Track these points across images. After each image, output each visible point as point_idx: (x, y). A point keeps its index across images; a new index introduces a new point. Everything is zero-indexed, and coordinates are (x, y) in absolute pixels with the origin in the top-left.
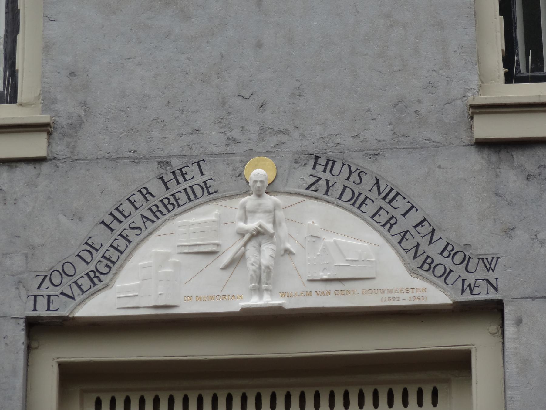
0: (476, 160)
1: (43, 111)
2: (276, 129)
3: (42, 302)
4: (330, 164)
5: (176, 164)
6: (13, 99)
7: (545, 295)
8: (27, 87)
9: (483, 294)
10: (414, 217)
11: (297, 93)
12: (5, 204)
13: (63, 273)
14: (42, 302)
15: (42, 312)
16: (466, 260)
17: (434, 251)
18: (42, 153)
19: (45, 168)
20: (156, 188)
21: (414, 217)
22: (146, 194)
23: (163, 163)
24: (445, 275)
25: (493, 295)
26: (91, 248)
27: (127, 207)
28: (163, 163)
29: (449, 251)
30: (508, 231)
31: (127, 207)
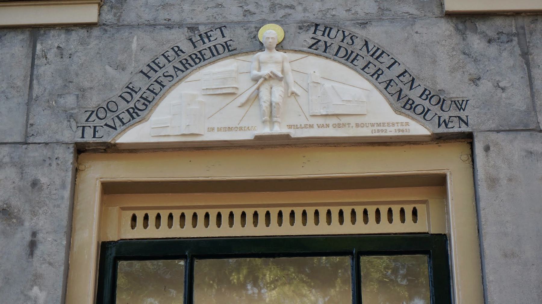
0: (446, 27)
2: (284, 4)
3: (89, 132)
4: (327, 29)
5: (202, 29)
9: (456, 128)
10: (397, 70)
14: (89, 132)
15: (89, 138)
19: (96, 32)
20: (187, 47)
21: (397, 70)
22: (178, 51)
25: (464, 129)
26: (131, 90)
27: (162, 61)
28: (192, 28)
29: (426, 94)
31: (162, 61)
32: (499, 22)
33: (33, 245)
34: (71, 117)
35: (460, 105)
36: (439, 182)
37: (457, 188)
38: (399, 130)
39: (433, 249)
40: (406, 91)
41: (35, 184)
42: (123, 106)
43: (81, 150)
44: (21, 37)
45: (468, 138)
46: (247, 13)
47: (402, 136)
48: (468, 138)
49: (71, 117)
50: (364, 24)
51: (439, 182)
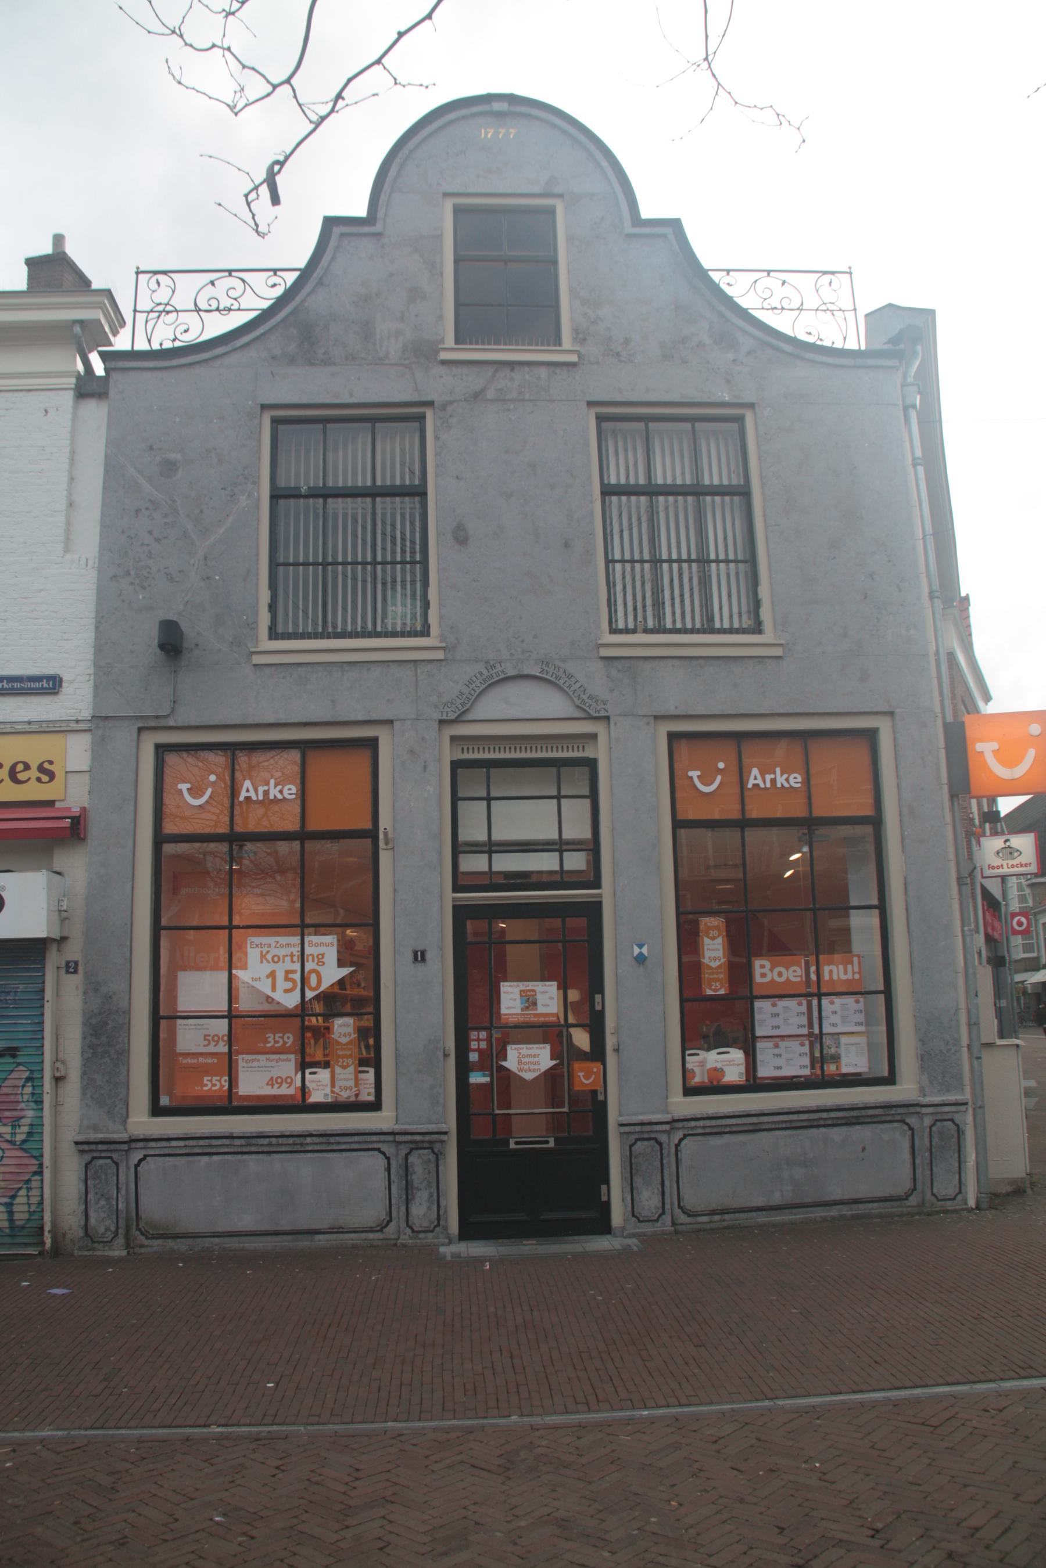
0: (600, 664)
1: (441, 641)
2: (304, 490)
3: (445, 714)
4: (548, 664)
5: (492, 663)
6: (428, 635)
7: (3, 394)
8: (434, 630)
9: (603, 714)
10: (578, 685)
11: (535, 637)
12: (172, 644)
13: (452, 703)
14: (445, 714)
15: (444, 717)
16: (597, 701)
17: (585, 697)
18: (442, 658)
19: (444, 663)
20: (485, 672)
21: (578, 685)
22: (481, 674)
23: (487, 662)
24: (775, 342)
25: (606, 714)
26: (462, 694)
27: (474, 679)
28: (487, 662)
29: (591, 697)
30: (612, 690)
31: (474, 679)
32: (623, 661)
33: (425, 767)
34: (436, 706)
35: (605, 703)
36: (594, 737)
37: (602, 739)
38: (253, 1061)
39: (591, 764)
40: (582, 696)
41: (423, 738)
42: (459, 701)
43: (441, 722)
44: (411, 665)
45: (608, 718)
46: (511, 654)
47: (274, 1097)
48: (608, 718)
49: (436, 706)
50: (564, 661)
51: (594, 737)
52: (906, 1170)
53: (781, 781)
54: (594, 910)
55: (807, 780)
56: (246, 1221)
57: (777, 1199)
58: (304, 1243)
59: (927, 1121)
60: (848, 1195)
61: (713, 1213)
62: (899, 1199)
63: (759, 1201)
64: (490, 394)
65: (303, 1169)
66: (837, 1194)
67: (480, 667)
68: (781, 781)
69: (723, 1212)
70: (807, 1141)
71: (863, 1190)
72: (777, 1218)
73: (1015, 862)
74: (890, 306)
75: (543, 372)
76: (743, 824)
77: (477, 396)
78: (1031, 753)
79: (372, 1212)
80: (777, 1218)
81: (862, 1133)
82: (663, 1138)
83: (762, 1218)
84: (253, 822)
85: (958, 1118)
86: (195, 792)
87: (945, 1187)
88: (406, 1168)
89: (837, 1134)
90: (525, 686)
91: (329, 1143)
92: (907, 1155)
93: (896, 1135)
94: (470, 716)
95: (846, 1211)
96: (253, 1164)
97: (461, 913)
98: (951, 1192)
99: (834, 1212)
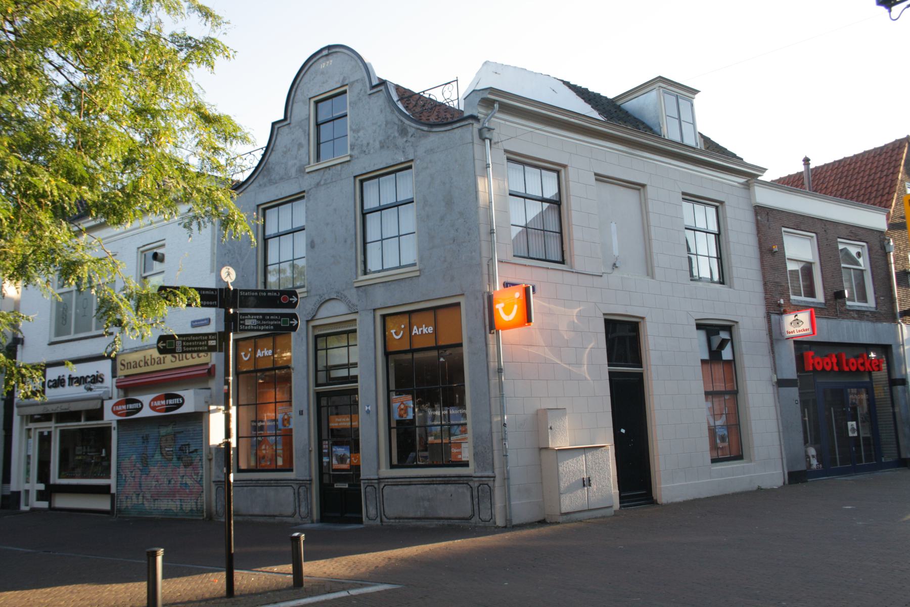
36: (355, 320)
52: (469, 506)
53: (425, 331)
54: (609, 365)
55: (435, 330)
56: (257, 511)
57: (419, 514)
58: (271, 520)
59: (476, 484)
60: (447, 515)
61: (396, 518)
62: (467, 519)
63: (411, 515)
64: (322, 183)
65: (271, 492)
66: (442, 515)
67: (318, 297)
68: (425, 331)
69: (400, 518)
70: (428, 491)
71: (452, 514)
72: (419, 523)
73: (800, 328)
74: (660, 77)
75: (339, 167)
76: (412, 351)
77: (318, 184)
78: (516, 307)
79: (290, 510)
80: (419, 523)
81: (450, 488)
82: (376, 486)
83: (414, 523)
84: (262, 365)
85: (491, 484)
86: (246, 356)
87: (485, 515)
88: (299, 493)
89: (441, 488)
90: (333, 302)
91: (278, 483)
92: (469, 499)
93: (464, 490)
94: (317, 317)
95: (446, 522)
96: (258, 490)
97: (319, 395)
98: (488, 518)
99: (441, 522)
